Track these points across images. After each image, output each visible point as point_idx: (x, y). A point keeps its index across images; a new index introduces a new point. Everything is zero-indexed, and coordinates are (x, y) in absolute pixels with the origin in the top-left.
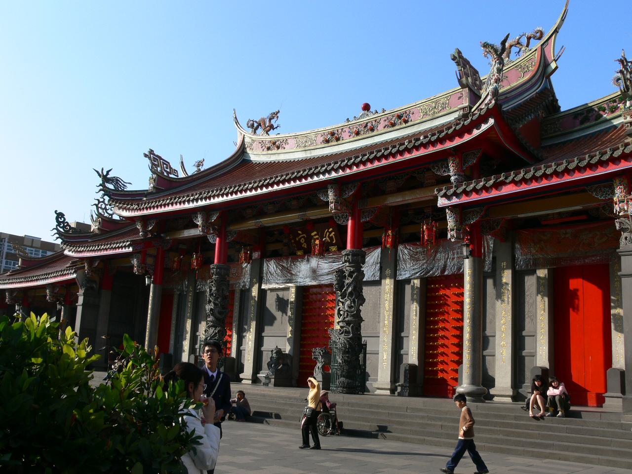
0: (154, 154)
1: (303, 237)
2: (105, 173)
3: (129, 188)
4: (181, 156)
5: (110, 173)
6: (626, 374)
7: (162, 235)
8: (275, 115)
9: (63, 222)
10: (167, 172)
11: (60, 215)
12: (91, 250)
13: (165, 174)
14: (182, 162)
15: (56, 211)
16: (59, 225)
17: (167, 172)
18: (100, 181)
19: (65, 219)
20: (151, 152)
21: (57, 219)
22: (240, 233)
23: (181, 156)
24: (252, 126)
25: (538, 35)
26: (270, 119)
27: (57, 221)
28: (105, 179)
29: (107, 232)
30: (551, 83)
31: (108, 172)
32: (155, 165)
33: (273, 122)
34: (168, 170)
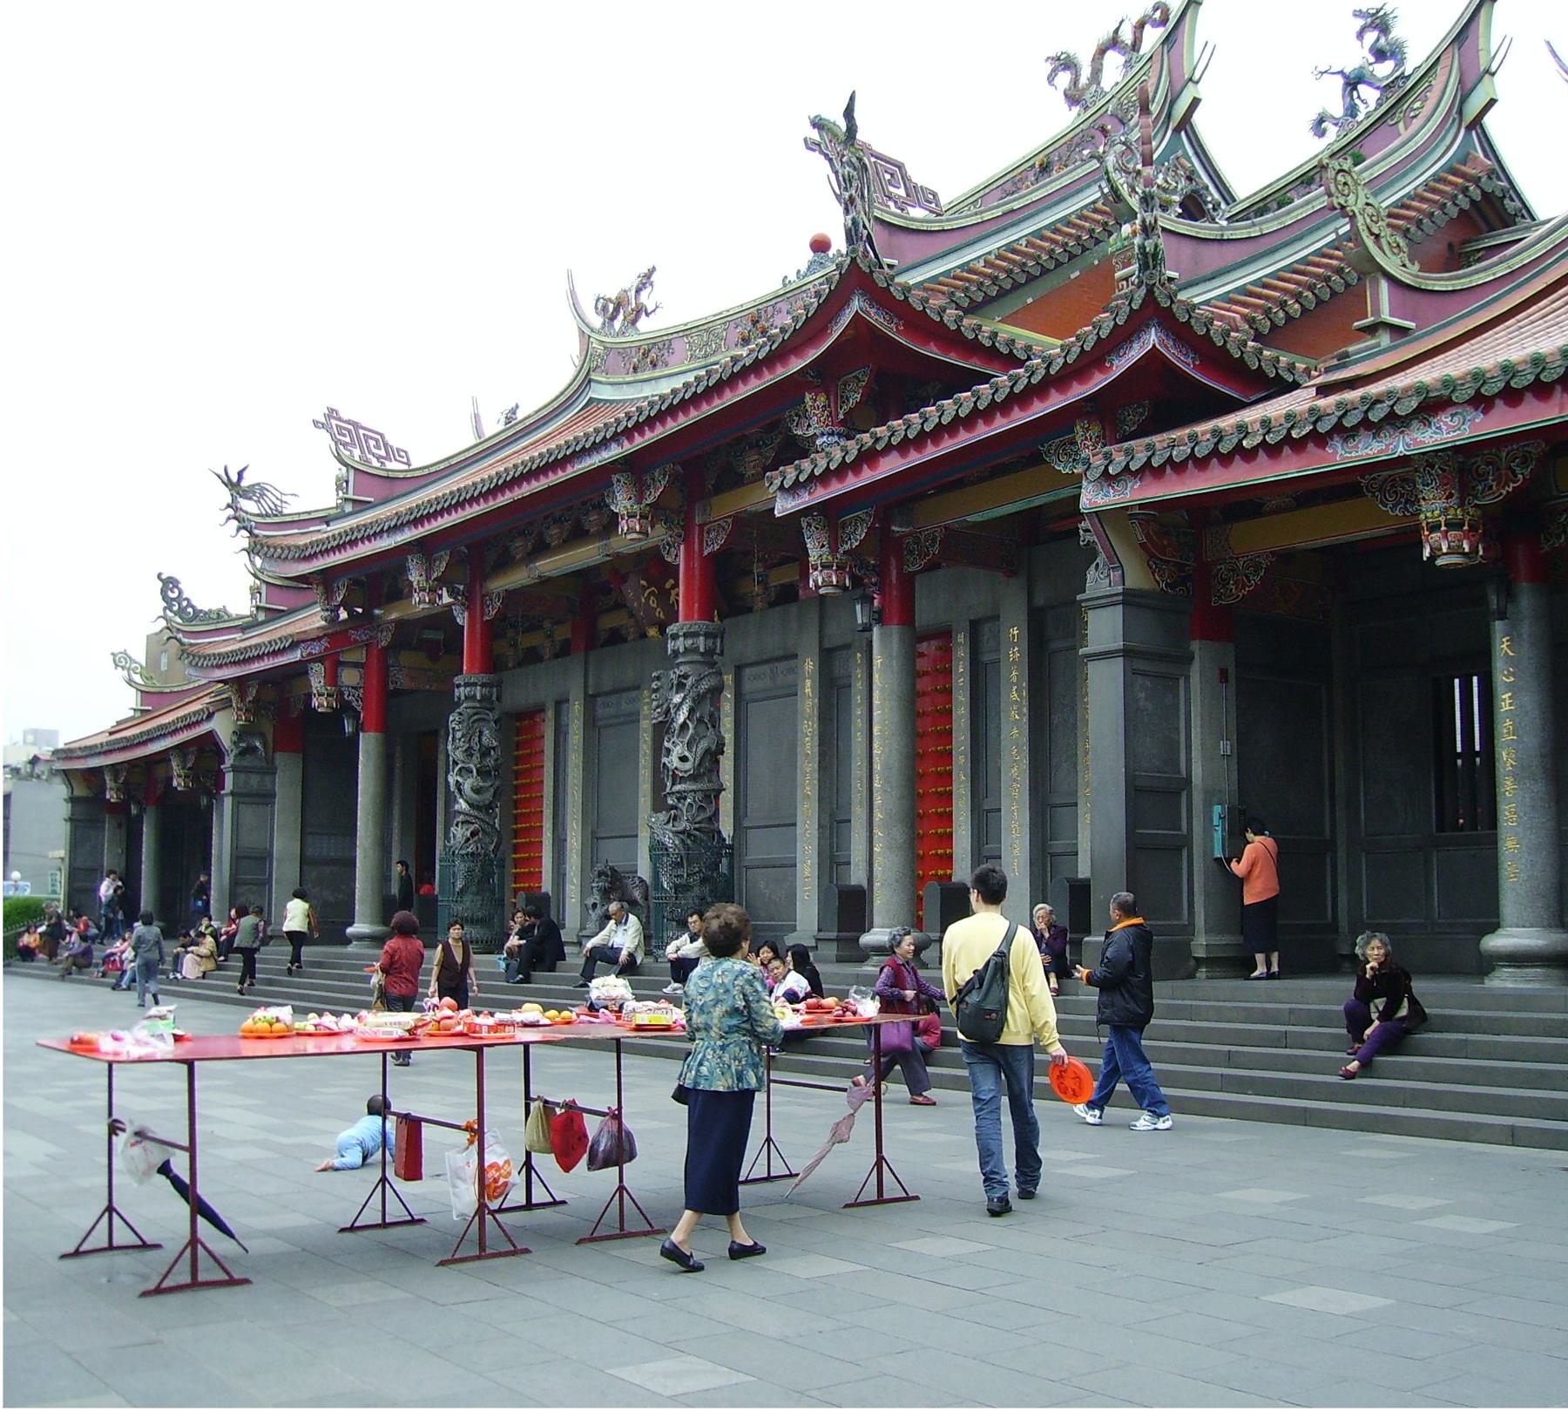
0: (340, 419)
1: (652, 593)
2: (234, 478)
3: (294, 507)
4: (475, 402)
5: (245, 474)
6: (1096, 896)
7: (377, 612)
8: (646, 280)
9: (179, 599)
10: (378, 458)
11: (169, 584)
12: (812, 478)
13: (375, 463)
14: (477, 417)
15: (159, 576)
16: (169, 607)
17: (378, 458)
18: (225, 495)
19: (180, 592)
20: (332, 413)
21: (163, 593)
22: (510, 595)
23: (475, 402)
24: (605, 308)
25: (1157, 15)
26: (638, 291)
27: (165, 597)
28: (234, 486)
29: (279, 614)
30: (1201, 146)
31: (240, 474)
32: (345, 445)
33: (644, 294)
34: (382, 453)
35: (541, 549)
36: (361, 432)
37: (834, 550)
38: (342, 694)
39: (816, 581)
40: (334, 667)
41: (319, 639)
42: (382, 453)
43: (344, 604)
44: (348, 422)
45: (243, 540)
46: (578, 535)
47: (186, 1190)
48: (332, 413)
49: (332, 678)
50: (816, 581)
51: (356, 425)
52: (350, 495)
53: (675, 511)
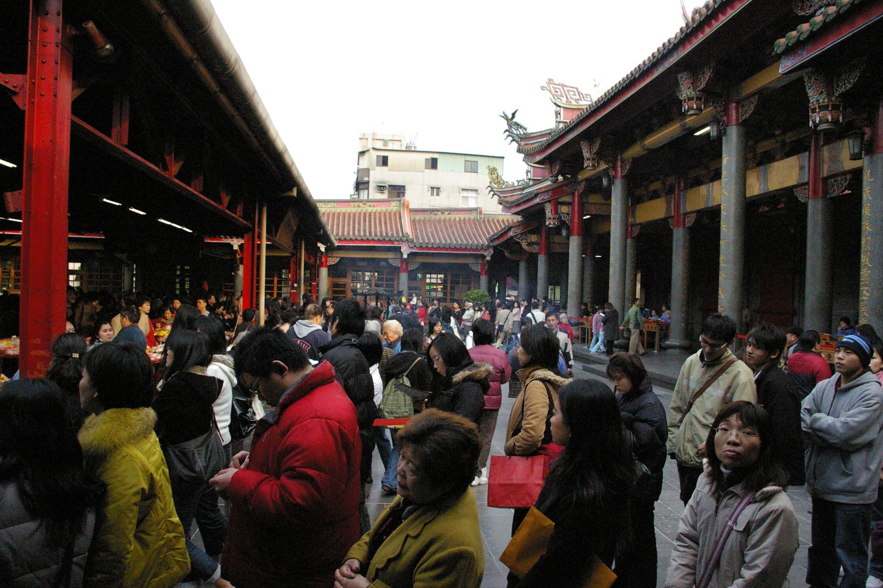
2: (510, 116)
13: (574, 102)
20: (550, 81)
34: (578, 97)
35: (650, 131)
36: (566, 88)
37: (829, 95)
38: (560, 217)
39: (814, 122)
40: (557, 204)
41: (547, 191)
42: (578, 97)
43: (560, 172)
44: (559, 85)
45: (515, 145)
46: (667, 121)
47: (716, 512)
48: (550, 81)
49: (556, 211)
50: (814, 122)
51: (563, 86)
52: (562, 120)
53: (716, 94)
